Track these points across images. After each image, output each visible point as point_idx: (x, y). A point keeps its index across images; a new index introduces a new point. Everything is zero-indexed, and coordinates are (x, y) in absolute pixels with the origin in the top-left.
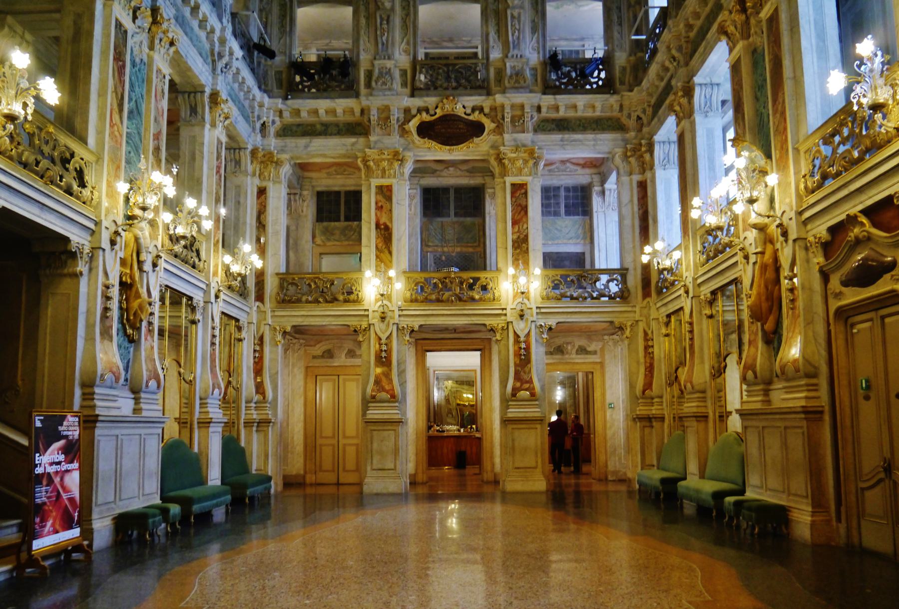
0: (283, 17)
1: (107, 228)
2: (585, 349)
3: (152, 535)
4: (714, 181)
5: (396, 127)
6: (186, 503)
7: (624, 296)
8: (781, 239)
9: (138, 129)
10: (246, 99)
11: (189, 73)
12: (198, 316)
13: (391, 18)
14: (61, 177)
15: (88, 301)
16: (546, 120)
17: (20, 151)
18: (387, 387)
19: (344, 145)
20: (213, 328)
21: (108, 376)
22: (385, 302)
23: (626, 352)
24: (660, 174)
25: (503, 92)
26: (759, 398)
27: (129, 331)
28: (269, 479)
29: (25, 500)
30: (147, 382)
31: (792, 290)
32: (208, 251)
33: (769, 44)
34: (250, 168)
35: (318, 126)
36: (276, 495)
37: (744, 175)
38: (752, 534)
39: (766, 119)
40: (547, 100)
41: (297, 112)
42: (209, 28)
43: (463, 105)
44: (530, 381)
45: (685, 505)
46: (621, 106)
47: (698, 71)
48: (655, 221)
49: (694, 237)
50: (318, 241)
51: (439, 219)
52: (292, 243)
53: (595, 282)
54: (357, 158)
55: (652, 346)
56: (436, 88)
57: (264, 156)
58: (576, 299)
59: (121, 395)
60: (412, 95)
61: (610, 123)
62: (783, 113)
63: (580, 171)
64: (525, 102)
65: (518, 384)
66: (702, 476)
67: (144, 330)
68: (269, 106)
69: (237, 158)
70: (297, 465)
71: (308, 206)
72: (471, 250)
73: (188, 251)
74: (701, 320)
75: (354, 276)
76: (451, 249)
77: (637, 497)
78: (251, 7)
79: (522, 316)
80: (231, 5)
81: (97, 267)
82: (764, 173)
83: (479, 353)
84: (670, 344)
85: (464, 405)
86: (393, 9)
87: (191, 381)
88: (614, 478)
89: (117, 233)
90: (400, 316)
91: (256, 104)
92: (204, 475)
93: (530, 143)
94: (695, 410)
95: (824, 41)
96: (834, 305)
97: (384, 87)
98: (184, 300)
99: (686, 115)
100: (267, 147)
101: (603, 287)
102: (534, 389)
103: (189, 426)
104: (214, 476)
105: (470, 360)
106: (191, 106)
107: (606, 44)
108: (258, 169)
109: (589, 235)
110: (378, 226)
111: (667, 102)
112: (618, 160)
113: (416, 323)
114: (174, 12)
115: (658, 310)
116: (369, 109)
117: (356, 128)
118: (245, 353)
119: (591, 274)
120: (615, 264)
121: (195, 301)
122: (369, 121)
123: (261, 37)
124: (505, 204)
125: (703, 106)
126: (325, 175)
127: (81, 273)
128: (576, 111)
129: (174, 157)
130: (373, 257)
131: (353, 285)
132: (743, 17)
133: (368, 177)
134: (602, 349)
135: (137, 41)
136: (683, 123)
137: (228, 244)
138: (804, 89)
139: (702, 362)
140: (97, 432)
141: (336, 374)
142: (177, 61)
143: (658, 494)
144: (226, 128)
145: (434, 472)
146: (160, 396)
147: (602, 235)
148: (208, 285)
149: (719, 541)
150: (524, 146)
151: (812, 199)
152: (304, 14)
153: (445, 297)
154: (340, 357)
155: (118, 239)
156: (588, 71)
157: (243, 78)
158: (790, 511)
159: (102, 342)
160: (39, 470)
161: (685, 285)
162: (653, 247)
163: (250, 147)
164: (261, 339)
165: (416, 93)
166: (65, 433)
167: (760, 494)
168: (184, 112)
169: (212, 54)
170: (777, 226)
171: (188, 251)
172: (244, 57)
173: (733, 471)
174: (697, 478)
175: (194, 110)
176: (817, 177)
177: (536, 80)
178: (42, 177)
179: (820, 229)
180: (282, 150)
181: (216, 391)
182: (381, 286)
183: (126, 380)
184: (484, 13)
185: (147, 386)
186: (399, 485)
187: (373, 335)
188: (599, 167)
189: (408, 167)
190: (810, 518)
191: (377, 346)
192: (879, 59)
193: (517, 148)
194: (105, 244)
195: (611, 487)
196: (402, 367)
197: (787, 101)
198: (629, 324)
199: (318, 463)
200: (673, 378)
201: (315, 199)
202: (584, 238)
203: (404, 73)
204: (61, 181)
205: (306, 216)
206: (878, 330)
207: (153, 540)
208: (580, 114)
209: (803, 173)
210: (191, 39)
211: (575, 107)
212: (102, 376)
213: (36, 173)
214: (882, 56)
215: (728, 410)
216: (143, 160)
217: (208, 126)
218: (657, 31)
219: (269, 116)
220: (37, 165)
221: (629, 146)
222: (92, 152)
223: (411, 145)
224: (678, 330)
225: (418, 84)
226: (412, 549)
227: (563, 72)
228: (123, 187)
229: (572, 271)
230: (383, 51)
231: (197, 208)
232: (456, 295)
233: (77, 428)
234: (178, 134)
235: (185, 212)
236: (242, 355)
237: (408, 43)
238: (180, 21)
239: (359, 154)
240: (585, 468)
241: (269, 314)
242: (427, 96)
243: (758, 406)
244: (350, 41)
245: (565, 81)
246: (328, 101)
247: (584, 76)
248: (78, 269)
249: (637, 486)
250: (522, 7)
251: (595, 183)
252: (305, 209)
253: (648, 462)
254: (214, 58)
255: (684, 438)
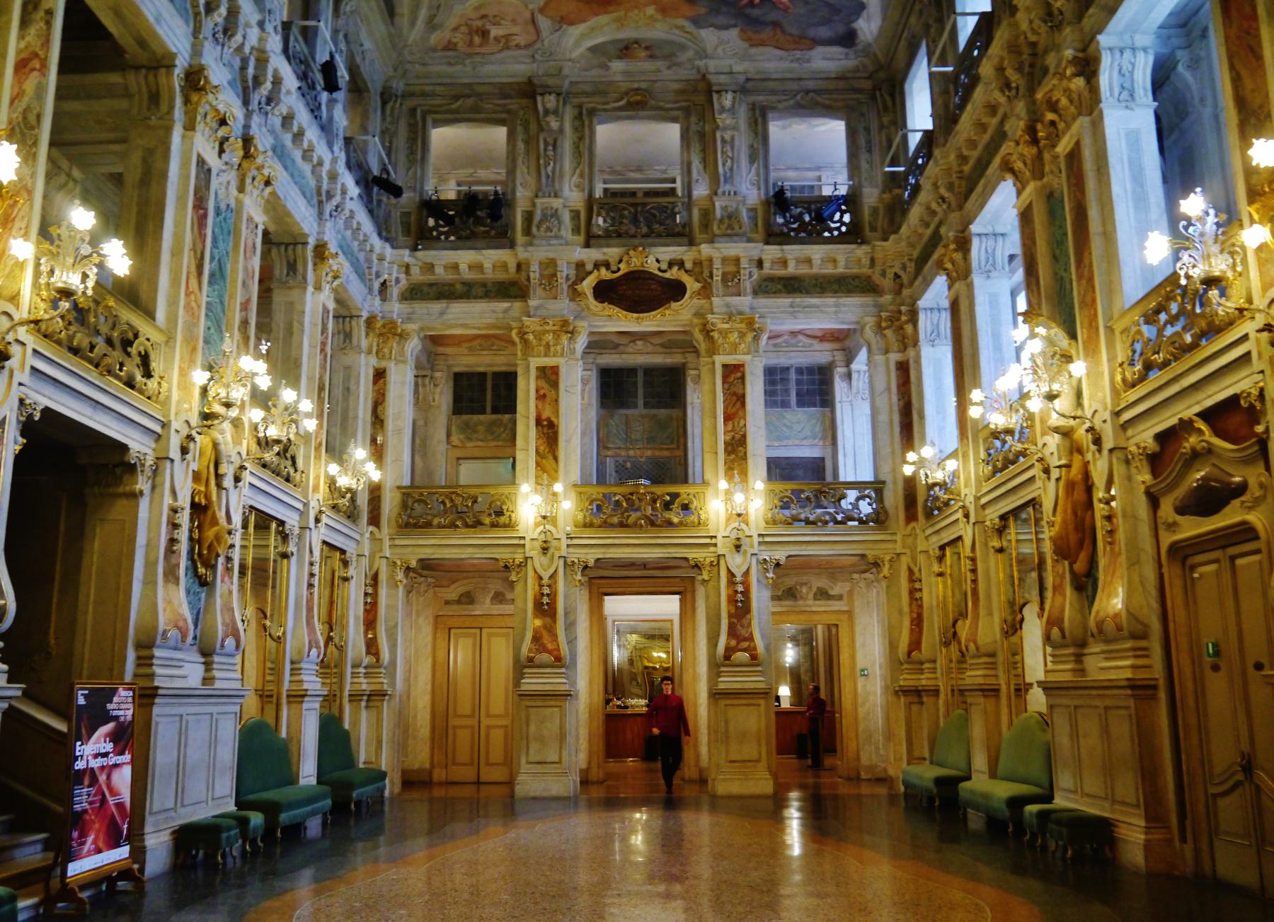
0: (412, 140)
1: (177, 431)
2: (826, 593)
3: (224, 857)
4: (1001, 371)
5: (565, 286)
6: (271, 810)
7: (879, 519)
8: (1093, 448)
9: (221, 297)
10: (361, 250)
11: (288, 220)
12: (292, 548)
13: (559, 142)
14: (122, 365)
15: (149, 529)
16: (770, 279)
17: (70, 333)
18: (550, 646)
19: (494, 312)
20: (312, 564)
21: (173, 633)
22: (548, 527)
23: (883, 597)
24: (927, 352)
25: (711, 241)
26: (1069, 666)
27: (202, 570)
28: (382, 776)
29: (60, 809)
30: (223, 641)
31: (1109, 518)
32: (307, 458)
33: (1069, 188)
34: (364, 343)
35: (458, 286)
36: (392, 799)
37: (1039, 361)
38: (1064, 859)
39: (1068, 286)
40: (771, 252)
41: (430, 267)
42: (315, 160)
43: (657, 258)
44: (750, 638)
45: (969, 816)
46: (873, 260)
47: (975, 218)
48: (922, 416)
49: (975, 441)
50: (455, 439)
51: (623, 411)
52: (420, 445)
53: (840, 500)
54: (511, 329)
55: (921, 590)
56: (619, 235)
57: (384, 326)
58: (813, 523)
59: (188, 658)
60: (587, 245)
61: (857, 282)
62: (1091, 280)
63: (817, 345)
64: (741, 255)
65: (733, 643)
66: (993, 774)
67: (220, 568)
68: (392, 260)
69: (348, 329)
70: (420, 757)
71: (441, 393)
72: (666, 453)
73: (281, 460)
74: (987, 554)
75: (506, 490)
76: (638, 453)
77: (903, 804)
78: (370, 128)
79: (738, 547)
80: (345, 129)
81: (163, 483)
82: (1068, 358)
83: (677, 597)
84: (945, 587)
85: (655, 668)
86: (561, 130)
87: (279, 638)
88: (869, 776)
89: (190, 438)
90: (568, 546)
91: (374, 257)
92: (295, 768)
93: (747, 310)
94: (981, 681)
95: (1142, 186)
96: (1167, 539)
97: (549, 234)
98: (274, 525)
99: (961, 275)
100: (388, 315)
101: (850, 507)
102: (755, 648)
103: (274, 700)
104: (308, 772)
105: (666, 606)
106: (288, 263)
107: (851, 177)
108: (375, 344)
109: (831, 434)
110: (539, 422)
111: (935, 256)
112: (869, 332)
113: (591, 556)
114: (271, 140)
115: (927, 539)
116: (528, 264)
117: (511, 289)
118: (353, 597)
119: (834, 489)
120: (867, 476)
121: (287, 527)
122: (528, 279)
123: (385, 170)
124: (714, 393)
125: (983, 263)
126: (466, 352)
127: (141, 493)
128: (811, 267)
129: (264, 329)
130: (532, 464)
131: (503, 503)
132: (1034, 150)
133: (526, 355)
134: (851, 592)
135: (223, 183)
136: (957, 285)
137: (335, 450)
138: (1117, 248)
139: (990, 614)
140: (156, 710)
141: (477, 627)
142: (274, 206)
143: (931, 800)
144: (335, 291)
145: (613, 766)
146: (238, 659)
147: (848, 433)
148: (306, 505)
149: (1018, 869)
150: (740, 313)
151: (1133, 395)
152: (442, 137)
153: (631, 521)
154: (484, 603)
155: (192, 445)
156: (826, 214)
157: (358, 223)
158: (1116, 826)
159: (165, 587)
160: (80, 765)
161: (963, 507)
162: (919, 454)
163: (365, 315)
164: (375, 578)
165: (592, 242)
166: (115, 713)
167: (1076, 802)
168: (279, 270)
169: (319, 193)
170: (1087, 431)
171: (281, 460)
172: (360, 196)
173: (1036, 769)
174: (986, 777)
175: (292, 267)
176: (1138, 367)
177: (756, 225)
178: (97, 366)
179: (1145, 436)
180: (409, 319)
181: (314, 652)
182: (542, 505)
183: (195, 638)
184: (685, 136)
185: (222, 646)
186: (565, 785)
187: (531, 574)
188: (844, 341)
189: (581, 342)
190: (1143, 837)
191: (537, 588)
192: (1211, 219)
193: (730, 317)
194: (175, 453)
195: (865, 790)
196: (572, 618)
197: (1095, 264)
198: (887, 558)
199: (450, 750)
200: (950, 634)
201: (451, 384)
202: (824, 438)
203: (576, 215)
204: (121, 370)
205: (439, 407)
206: (1227, 577)
207: (225, 864)
208: (815, 270)
209: (1120, 360)
210: (292, 175)
211: (809, 261)
212: (165, 632)
213: (90, 361)
214: (1216, 216)
215: (1028, 680)
216: (227, 340)
217: (310, 289)
218: (920, 161)
219: (392, 273)
220: (91, 351)
221: (884, 314)
222: (161, 330)
223: (584, 314)
224: (955, 567)
225: (595, 230)
226: (583, 878)
227: (793, 214)
228: (200, 377)
229: (806, 483)
230: (547, 185)
231: (297, 402)
232: (646, 517)
233: (131, 706)
234: (270, 297)
235: (281, 407)
236: (349, 599)
237: (582, 175)
238: (279, 152)
239: (514, 324)
240: (828, 762)
241: (387, 543)
242: (608, 246)
243: (1068, 677)
244: (503, 171)
245: (795, 226)
246: (472, 252)
247: (821, 219)
248: (138, 487)
249: (902, 789)
250: (735, 128)
251: (838, 363)
252: (437, 397)
253: (916, 754)
254: (321, 199)
255: (967, 720)
